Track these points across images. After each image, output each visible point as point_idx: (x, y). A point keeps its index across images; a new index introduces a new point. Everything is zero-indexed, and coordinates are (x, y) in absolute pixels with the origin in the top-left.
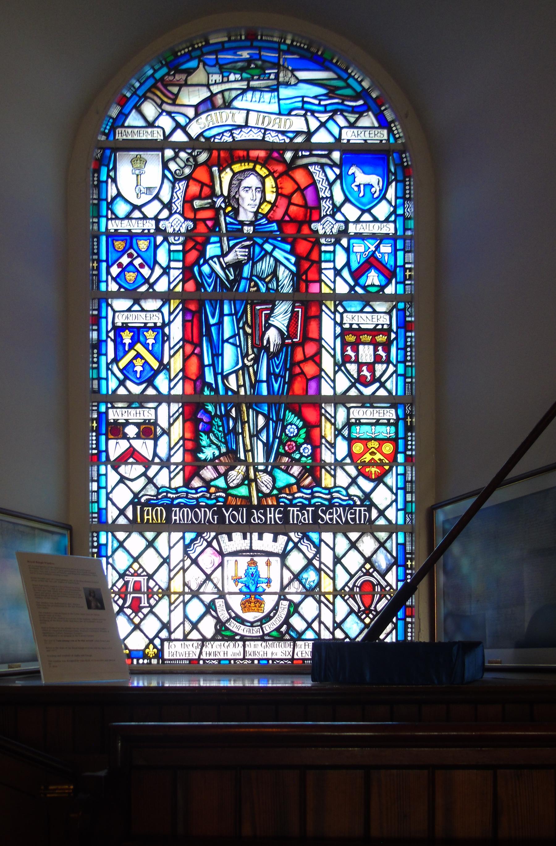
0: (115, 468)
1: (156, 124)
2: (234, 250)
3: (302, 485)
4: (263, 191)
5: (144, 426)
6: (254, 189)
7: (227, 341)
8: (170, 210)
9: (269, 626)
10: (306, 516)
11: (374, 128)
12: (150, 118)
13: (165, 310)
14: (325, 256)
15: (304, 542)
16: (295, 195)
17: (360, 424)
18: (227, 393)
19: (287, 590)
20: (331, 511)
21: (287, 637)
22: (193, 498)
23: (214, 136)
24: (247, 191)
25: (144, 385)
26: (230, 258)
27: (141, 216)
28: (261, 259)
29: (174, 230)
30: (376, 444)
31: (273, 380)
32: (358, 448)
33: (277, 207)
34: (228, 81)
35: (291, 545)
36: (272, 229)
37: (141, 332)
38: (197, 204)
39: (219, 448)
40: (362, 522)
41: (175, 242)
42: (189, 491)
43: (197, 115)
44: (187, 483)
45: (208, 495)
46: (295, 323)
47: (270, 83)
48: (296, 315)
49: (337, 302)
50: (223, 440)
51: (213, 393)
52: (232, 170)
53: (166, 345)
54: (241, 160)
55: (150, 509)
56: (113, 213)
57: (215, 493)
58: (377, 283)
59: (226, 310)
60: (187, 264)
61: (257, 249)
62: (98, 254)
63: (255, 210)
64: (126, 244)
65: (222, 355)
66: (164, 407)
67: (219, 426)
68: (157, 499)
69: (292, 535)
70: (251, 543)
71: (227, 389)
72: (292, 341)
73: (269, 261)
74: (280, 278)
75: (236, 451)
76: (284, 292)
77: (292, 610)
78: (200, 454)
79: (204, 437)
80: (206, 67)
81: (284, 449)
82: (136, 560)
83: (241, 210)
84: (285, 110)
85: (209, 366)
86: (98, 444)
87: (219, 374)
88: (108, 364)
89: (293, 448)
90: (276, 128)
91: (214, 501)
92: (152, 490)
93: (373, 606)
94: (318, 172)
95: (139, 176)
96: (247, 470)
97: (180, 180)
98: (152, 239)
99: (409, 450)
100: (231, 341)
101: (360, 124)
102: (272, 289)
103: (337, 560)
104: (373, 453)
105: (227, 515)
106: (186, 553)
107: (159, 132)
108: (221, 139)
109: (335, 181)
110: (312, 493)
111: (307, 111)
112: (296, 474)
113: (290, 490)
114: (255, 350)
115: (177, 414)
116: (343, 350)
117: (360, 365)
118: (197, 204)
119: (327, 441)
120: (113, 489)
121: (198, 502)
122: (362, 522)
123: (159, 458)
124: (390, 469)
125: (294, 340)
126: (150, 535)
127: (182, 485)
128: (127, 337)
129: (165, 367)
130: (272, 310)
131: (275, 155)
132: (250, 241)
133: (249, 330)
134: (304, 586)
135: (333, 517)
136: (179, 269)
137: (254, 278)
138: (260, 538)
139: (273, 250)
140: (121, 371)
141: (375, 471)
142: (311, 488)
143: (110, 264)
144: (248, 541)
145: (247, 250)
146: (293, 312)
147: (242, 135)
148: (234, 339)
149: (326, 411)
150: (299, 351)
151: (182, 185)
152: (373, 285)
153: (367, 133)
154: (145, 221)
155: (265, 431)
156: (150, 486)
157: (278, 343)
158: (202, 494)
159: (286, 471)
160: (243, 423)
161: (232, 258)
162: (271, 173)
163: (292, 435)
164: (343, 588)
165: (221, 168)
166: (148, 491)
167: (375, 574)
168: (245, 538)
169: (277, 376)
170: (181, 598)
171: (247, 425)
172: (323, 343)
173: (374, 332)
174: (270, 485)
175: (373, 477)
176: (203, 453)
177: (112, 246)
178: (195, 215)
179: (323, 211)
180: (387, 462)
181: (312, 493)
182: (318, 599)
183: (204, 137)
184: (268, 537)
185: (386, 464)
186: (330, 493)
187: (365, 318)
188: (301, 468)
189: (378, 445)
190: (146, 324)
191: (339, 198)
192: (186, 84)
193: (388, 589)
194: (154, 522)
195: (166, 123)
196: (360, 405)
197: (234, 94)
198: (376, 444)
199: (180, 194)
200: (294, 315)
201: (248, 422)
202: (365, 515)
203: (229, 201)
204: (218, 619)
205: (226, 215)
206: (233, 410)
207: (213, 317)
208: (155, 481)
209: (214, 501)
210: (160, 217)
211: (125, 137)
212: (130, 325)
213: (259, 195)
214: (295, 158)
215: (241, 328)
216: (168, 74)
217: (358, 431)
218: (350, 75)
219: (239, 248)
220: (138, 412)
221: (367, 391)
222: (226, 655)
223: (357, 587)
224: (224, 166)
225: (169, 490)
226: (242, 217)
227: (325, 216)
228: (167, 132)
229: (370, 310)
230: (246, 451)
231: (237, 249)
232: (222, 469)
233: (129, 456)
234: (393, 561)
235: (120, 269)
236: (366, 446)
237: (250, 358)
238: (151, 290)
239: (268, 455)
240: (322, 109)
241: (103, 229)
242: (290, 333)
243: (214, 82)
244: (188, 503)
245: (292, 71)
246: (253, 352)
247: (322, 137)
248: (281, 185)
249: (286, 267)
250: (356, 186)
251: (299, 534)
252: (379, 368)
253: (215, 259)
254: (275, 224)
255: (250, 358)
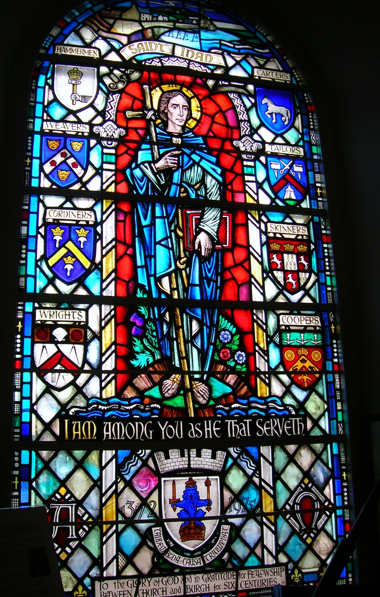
0: (41, 377)
1: (93, 45)
2: (164, 158)
3: (239, 395)
4: (190, 109)
5: (73, 329)
6: (181, 106)
7: (159, 243)
8: (104, 117)
9: (210, 554)
10: (244, 428)
11: (279, 71)
12: (88, 41)
13: (98, 209)
14: (247, 169)
15: (243, 458)
16: (217, 115)
17: (290, 331)
18: (160, 296)
19: (228, 514)
20: (269, 422)
21: (230, 566)
22: (127, 410)
23: (145, 60)
24: (175, 107)
25: (74, 285)
26: (161, 164)
27: (75, 120)
28: (190, 168)
29: (108, 135)
30: (304, 352)
31: (206, 284)
32: (289, 355)
33: (202, 124)
34: (157, 21)
35: (230, 461)
36: (198, 142)
37: (72, 230)
38: (129, 114)
39: (153, 354)
40: (299, 433)
41: (108, 146)
42: (122, 402)
43: (130, 42)
44: (119, 393)
45: (142, 407)
46: (224, 229)
47: (192, 26)
48: (224, 221)
49: (261, 212)
50: (157, 346)
51: (145, 296)
52: (161, 89)
53: (99, 244)
54: (169, 82)
55: (79, 422)
56: (48, 115)
57: (150, 404)
58: (293, 197)
59: (158, 213)
60: (119, 167)
61: (186, 159)
62: (31, 151)
63: (182, 124)
64: (60, 144)
65: (155, 256)
66: (95, 309)
67: (153, 331)
68: (87, 411)
69: (231, 450)
70: (189, 461)
71: (160, 291)
72: (222, 246)
73: (197, 170)
74: (208, 186)
75: (171, 358)
76: (212, 199)
77: (234, 534)
78: (133, 360)
79: (138, 342)
80: (139, 8)
81: (219, 356)
82: (63, 483)
83: (170, 123)
84: (207, 48)
85: (142, 267)
86: (22, 348)
87: (152, 276)
88: (37, 261)
89: (228, 355)
90: (198, 60)
91: (148, 414)
92: (82, 401)
93: (314, 524)
94: (236, 99)
95: (75, 85)
96: (183, 381)
97: (114, 93)
98: (86, 141)
99: (336, 357)
100: (163, 243)
101: (268, 66)
102: (201, 196)
103: (277, 476)
104: (303, 361)
105: (163, 429)
106: (119, 473)
107: (96, 52)
108: (151, 63)
109: (251, 108)
110: (249, 403)
111: (224, 51)
112: (232, 383)
113: (226, 401)
114: (187, 253)
115: (109, 317)
116: (270, 258)
117: (286, 273)
118: (129, 114)
119: (260, 348)
120: (38, 399)
121: (132, 415)
122: (299, 433)
123: (90, 364)
124: (321, 378)
125: (224, 245)
126: (79, 454)
127: (113, 395)
128: (58, 235)
129: (98, 267)
130: (202, 215)
131: (199, 81)
132: (179, 151)
133: (180, 234)
134: (245, 507)
135: (271, 429)
136: (111, 170)
137: (184, 184)
138: (199, 455)
139: (200, 161)
140: (50, 268)
141: (307, 379)
142: (248, 398)
143: (43, 162)
144: (186, 459)
145: (176, 159)
146: (221, 218)
147: (168, 63)
148: (166, 241)
149: (258, 317)
150: (229, 256)
151: (116, 97)
152: (290, 199)
153: (274, 74)
154: (79, 125)
155: (199, 336)
156: (79, 397)
157: (209, 248)
158: (135, 405)
159: (222, 380)
160: (177, 328)
161: (163, 165)
162: (196, 96)
163: (226, 341)
164: (284, 507)
165: (151, 87)
166: (76, 403)
167: (314, 489)
168: (182, 455)
169: (209, 281)
170: (114, 528)
171: (181, 330)
172: (251, 250)
173: (296, 241)
174: (207, 395)
175: (306, 386)
176: (137, 359)
177: (46, 145)
178: (127, 124)
179: (243, 131)
180: (317, 370)
181: (249, 403)
182: (260, 520)
183: (136, 60)
184: (206, 453)
185: (317, 372)
186: (266, 403)
187: (286, 229)
188: (237, 377)
189: (308, 352)
190: (78, 221)
191: (255, 122)
192: (121, 19)
193: (326, 504)
194: (84, 438)
195: (102, 45)
196: (288, 312)
197: (162, 30)
198: (305, 351)
199: (114, 104)
200: (222, 221)
201: (182, 327)
202: (301, 425)
203: (159, 115)
204: (154, 550)
205: (156, 126)
206: (167, 315)
207: (145, 218)
208: (84, 390)
209: (148, 414)
210: (94, 122)
211: (63, 53)
212: (61, 222)
213: (186, 112)
214: (216, 86)
215: (172, 231)
216: (105, 9)
217: (288, 338)
218: (257, 30)
219: (168, 156)
220: (67, 313)
221: (295, 298)
222: (164, 593)
223: (297, 504)
224: (154, 85)
225: (99, 401)
226: (171, 129)
227: (244, 136)
228: (103, 53)
229: (290, 221)
230: (180, 358)
231: (166, 156)
232: (157, 378)
233: (57, 362)
234: (330, 473)
235: (53, 167)
236: (296, 353)
237: (182, 261)
238: (83, 189)
239: (202, 362)
240: (236, 51)
241: (37, 128)
242: (220, 238)
243: (145, 19)
244: (121, 416)
245: (211, 21)
246: (186, 256)
247: (237, 72)
248: (205, 106)
249: (214, 177)
250: (269, 114)
251: (238, 449)
252: (303, 276)
253: (147, 164)
254: (200, 138)
255: (182, 261)
